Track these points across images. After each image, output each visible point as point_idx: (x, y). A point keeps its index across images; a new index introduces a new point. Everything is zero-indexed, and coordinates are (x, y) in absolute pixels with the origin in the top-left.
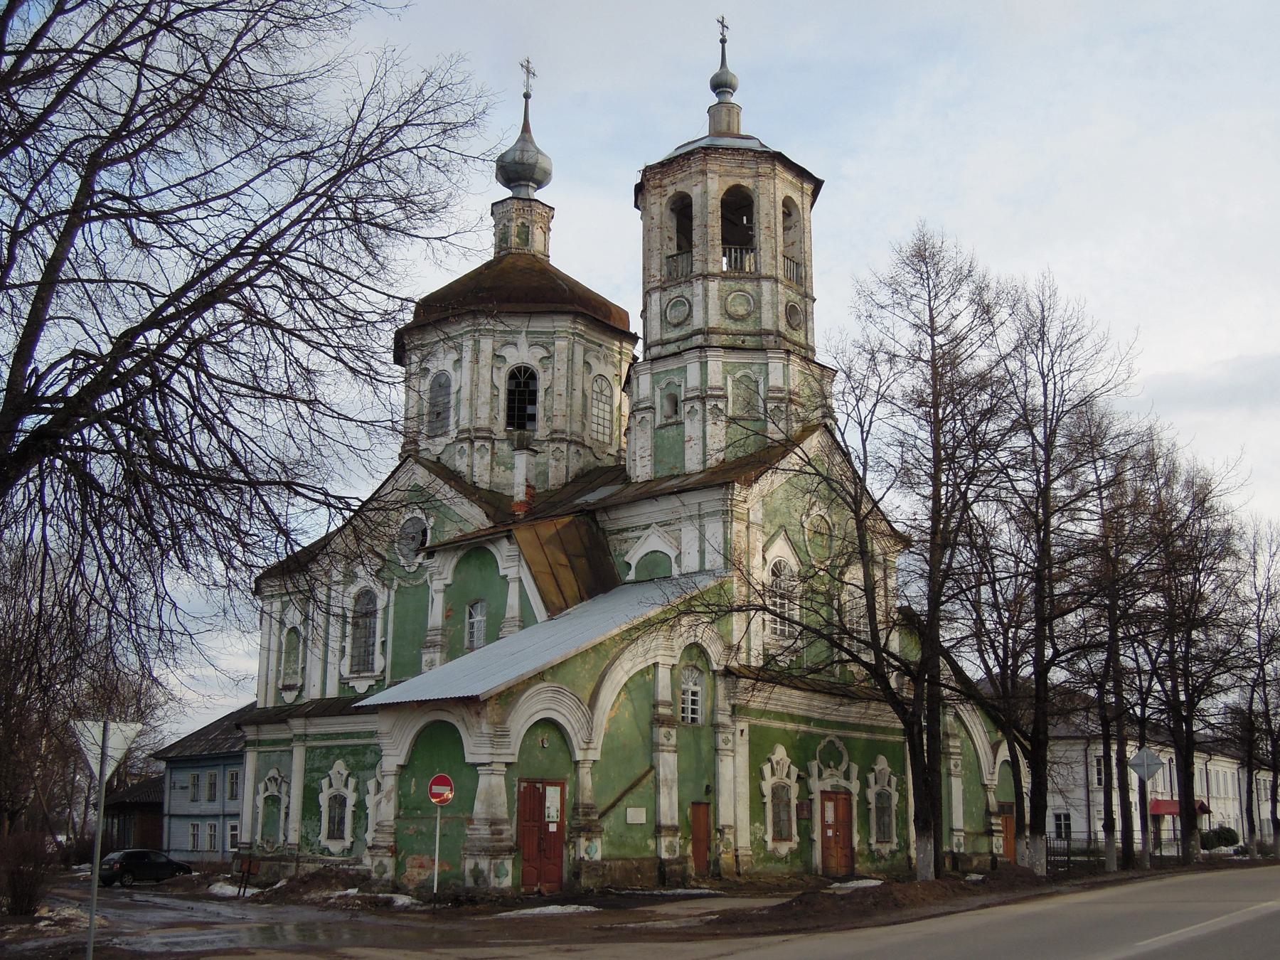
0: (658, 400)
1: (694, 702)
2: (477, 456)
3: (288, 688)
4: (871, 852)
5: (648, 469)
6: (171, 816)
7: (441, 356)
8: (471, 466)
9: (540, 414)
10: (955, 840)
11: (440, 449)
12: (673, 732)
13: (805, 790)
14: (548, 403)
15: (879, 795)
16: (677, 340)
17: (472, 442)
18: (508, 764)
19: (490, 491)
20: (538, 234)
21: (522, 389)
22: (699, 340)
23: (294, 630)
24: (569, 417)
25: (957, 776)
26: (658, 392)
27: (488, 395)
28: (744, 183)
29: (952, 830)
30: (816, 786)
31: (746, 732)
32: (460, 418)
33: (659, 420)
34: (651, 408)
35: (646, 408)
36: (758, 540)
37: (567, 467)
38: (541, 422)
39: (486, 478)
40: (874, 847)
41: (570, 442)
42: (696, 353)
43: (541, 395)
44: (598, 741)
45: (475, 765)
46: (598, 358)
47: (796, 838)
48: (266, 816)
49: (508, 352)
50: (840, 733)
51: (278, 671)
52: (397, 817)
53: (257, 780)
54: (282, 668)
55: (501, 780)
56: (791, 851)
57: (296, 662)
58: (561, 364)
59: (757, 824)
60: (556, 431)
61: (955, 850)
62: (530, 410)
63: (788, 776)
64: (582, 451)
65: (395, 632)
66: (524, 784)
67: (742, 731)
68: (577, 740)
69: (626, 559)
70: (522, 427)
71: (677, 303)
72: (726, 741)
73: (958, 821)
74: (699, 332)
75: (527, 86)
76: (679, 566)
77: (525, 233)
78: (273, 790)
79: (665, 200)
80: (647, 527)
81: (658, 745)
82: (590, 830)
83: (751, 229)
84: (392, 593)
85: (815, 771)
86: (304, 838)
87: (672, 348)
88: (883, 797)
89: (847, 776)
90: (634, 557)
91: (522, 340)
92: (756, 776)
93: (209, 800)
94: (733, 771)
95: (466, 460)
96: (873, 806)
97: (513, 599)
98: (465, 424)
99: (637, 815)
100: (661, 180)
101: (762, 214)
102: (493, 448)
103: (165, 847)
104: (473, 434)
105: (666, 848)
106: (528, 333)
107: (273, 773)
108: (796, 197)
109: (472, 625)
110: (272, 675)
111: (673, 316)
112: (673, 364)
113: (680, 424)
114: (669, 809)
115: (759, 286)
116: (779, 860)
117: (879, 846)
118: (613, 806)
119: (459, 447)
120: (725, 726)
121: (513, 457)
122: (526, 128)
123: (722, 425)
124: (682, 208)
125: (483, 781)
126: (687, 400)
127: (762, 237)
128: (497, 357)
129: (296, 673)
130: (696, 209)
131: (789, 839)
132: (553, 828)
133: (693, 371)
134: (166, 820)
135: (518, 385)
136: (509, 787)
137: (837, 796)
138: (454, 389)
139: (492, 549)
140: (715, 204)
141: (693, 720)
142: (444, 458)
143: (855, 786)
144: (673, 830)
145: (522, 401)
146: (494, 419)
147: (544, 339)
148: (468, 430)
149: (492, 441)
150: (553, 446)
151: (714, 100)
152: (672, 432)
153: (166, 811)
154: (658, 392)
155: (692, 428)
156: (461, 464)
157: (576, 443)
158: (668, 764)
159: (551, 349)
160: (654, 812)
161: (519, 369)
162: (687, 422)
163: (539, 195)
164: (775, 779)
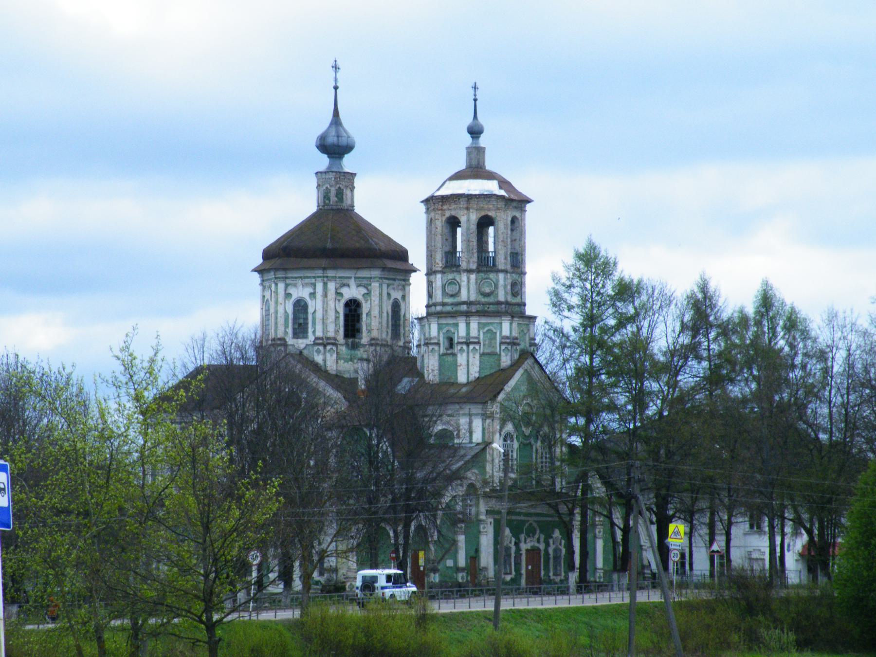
0: (441, 339)
2: (328, 355)
4: (551, 580)
8: (325, 361)
9: (364, 328)
10: (598, 575)
11: (302, 346)
13: (518, 549)
15: (555, 551)
16: (452, 304)
17: (325, 346)
19: (337, 376)
20: (348, 192)
24: (380, 330)
26: (441, 335)
28: (490, 214)
29: (596, 569)
30: (524, 547)
32: (316, 330)
34: (438, 344)
39: (335, 368)
40: (552, 577)
41: (382, 345)
43: (364, 316)
47: (514, 573)
49: (344, 290)
50: (536, 519)
56: (512, 579)
71: (453, 282)
72: (484, 528)
73: (600, 563)
74: (464, 303)
77: (340, 194)
79: (444, 218)
82: (435, 570)
85: (523, 539)
88: (557, 550)
89: (538, 541)
91: (352, 282)
96: (551, 556)
98: (319, 334)
99: (450, 563)
105: (461, 577)
106: (355, 278)
111: (450, 290)
114: (462, 562)
117: (554, 577)
120: (483, 521)
123: (477, 356)
126: (459, 343)
128: (288, 295)
131: (511, 573)
132: (422, 569)
133: (462, 327)
135: (350, 310)
137: (533, 553)
138: (311, 310)
142: (305, 352)
143: (542, 546)
145: (353, 321)
146: (337, 332)
147: (365, 282)
148: (322, 339)
151: (468, 140)
154: (441, 335)
155: (461, 359)
156: (319, 359)
160: (456, 562)
161: (351, 300)
162: (459, 355)
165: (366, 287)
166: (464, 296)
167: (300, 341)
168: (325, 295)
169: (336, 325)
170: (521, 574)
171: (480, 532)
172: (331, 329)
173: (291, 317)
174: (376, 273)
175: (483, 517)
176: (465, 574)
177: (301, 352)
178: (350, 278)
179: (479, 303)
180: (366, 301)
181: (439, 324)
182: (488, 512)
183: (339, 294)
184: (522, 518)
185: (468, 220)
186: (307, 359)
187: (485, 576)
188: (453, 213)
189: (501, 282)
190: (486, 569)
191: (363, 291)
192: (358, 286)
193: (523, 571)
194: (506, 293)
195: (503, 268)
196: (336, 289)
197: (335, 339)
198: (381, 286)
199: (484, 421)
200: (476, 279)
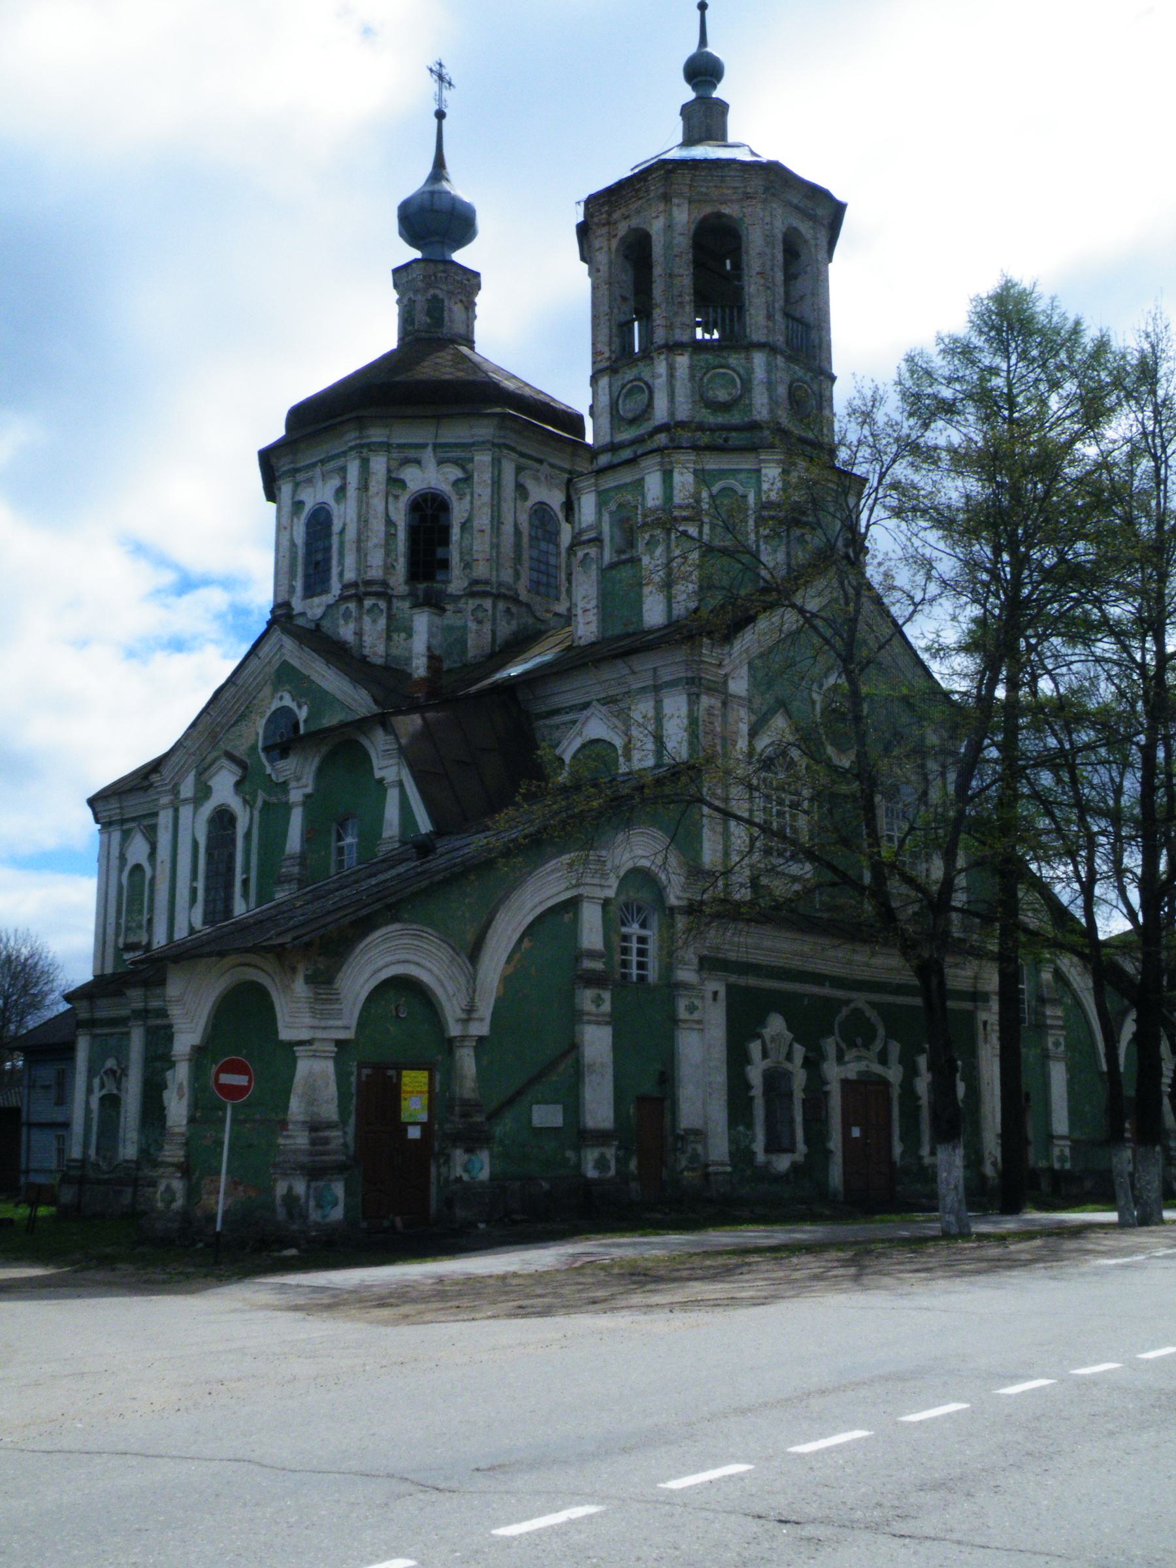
0: (606, 528)
1: (642, 953)
2: (367, 619)
3: (129, 947)
5: (593, 627)
6: (30, 1125)
7: (320, 483)
8: (359, 634)
10: (1056, 1152)
11: (319, 612)
12: (607, 995)
14: (466, 542)
17: (359, 599)
18: (339, 1043)
21: (429, 521)
22: (662, 439)
23: (138, 868)
24: (495, 561)
25: (1058, 1059)
26: (606, 518)
27: (382, 535)
28: (726, 210)
29: (1051, 1137)
30: (834, 1072)
31: (722, 994)
32: (345, 568)
33: (608, 556)
34: (598, 540)
35: (590, 541)
36: (742, 721)
37: (494, 632)
38: (456, 569)
39: (381, 649)
41: (497, 597)
42: (655, 459)
43: (455, 531)
44: (485, 1009)
45: (292, 1044)
46: (537, 479)
47: (801, 1147)
48: (102, 1123)
51: (118, 924)
52: (192, 1120)
53: (91, 1073)
54: (123, 921)
55: (329, 1066)
56: (795, 1166)
57: (140, 912)
58: (483, 491)
59: (741, 1128)
60: (476, 582)
61: (1057, 1166)
62: (440, 552)
63: (789, 1057)
64: (514, 610)
65: (261, 866)
66: (366, 1071)
67: (715, 994)
68: (452, 1010)
69: (558, 752)
70: (429, 576)
72: (692, 1009)
73: (1060, 1124)
74: (659, 429)
75: (440, 100)
76: (628, 758)
78: (111, 1088)
79: (614, 243)
80: (586, 706)
81: (582, 1013)
82: (473, 1140)
83: (739, 277)
84: (256, 814)
86: (144, 1152)
87: (626, 454)
89: (883, 1059)
90: (569, 749)
91: (428, 456)
92: (737, 1059)
93: (56, 1104)
94: (700, 1051)
95: (352, 626)
97: (392, 812)
98: (350, 575)
99: (547, 1116)
100: (609, 214)
101: (753, 253)
102: (389, 608)
103: (23, 1167)
104: (362, 589)
106: (436, 446)
107: (110, 1063)
108: (805, 228)
109: (341, 851)
110: (111, 931)
111: (628, 408)
112: (625, 476)
113: (635, 561)
114: (599, 1110)
115: (749, 359)
116: (778, 1178)
118: (510, 1102)
119: (343, 608)
121: (411, 615)
122: (439, 163)
124: (637, 251)
125: (304, 1067)
127: (753, 288)
128: (395, 482)
129: (140, 927)
130: (657, 250)
131: (792, 1149)
132: (414, 1133)
133: (653, 485)
134: (24, 1130)
136: (342, 1076)
137: (865, 1095)
138: (336, 527)
139: (366, 743)
140: (683, 242)
141: (642, 978)
142: (326, 624)
143: (894, 1074)
144: (601, 1137)
146: (389, 568)
148: (355, 584)
149: (389, 598)
150: (472, 603)
151: (688, 94)
152: (625, 573)
153: (24, 1119)
156: (347, 632)
157: (505, 597)
158: (597, 1043)
159: (470, 466)
160: (574, 1108)
163: (461, 256)
164: (767, 1063)
165: (460, 463)
166: (661, 412)
167: (316, 600)
168: (364, 487)
169: (387, 554)
170: (828, 1153)
171: (675, 1021)
172: (376, 559)
173: (301, 551)
174: (484, 431)
175: (686, 975)
176: (610, 1153)
177: (318, 626)
178: (424, 446)
179: (701, 427)
180: (461, 496)
181: (599, 493)
182: (709, 964)
183: (395, 482)
184: (826, 991)
185: (669, 227)
186: (328, 637)
187: (695, 1157)
188: (635, 222)
189: (760, 373)
190: (699, 1134)
191: (455, 473)
192: (441, 462)
193: (835, 1143)
194: (773, 402)
195: (763, 339)
196: (389, 471)
197: (384, 583)
198: (496, 463)
199: (693, 699)
200: (692, 367)
